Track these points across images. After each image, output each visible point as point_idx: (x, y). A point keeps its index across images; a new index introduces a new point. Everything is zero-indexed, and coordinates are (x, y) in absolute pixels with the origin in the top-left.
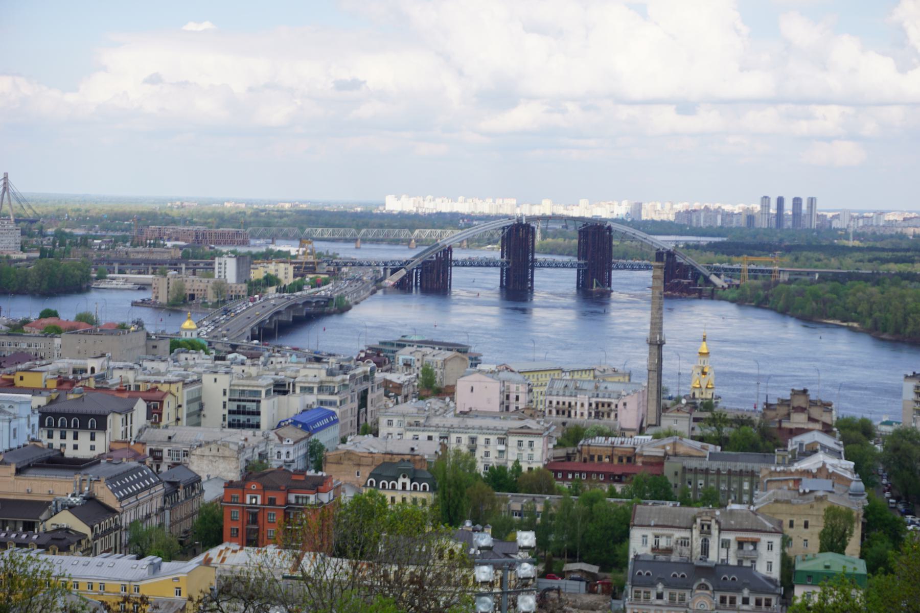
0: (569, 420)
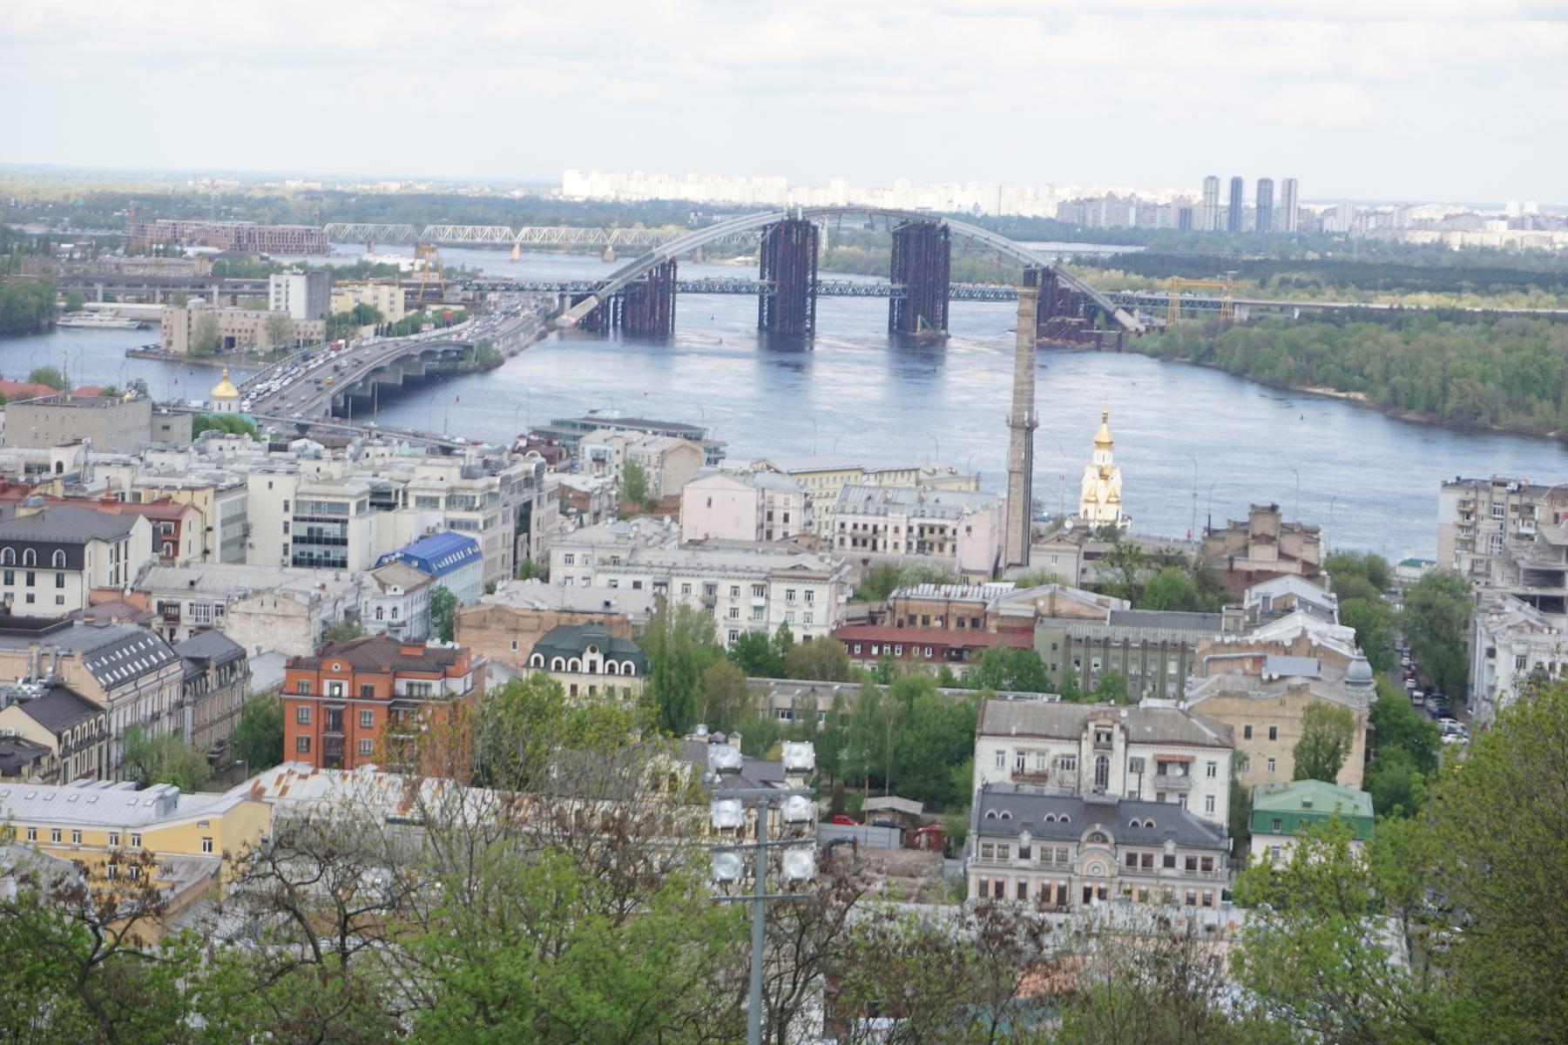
0: (873, 555)
